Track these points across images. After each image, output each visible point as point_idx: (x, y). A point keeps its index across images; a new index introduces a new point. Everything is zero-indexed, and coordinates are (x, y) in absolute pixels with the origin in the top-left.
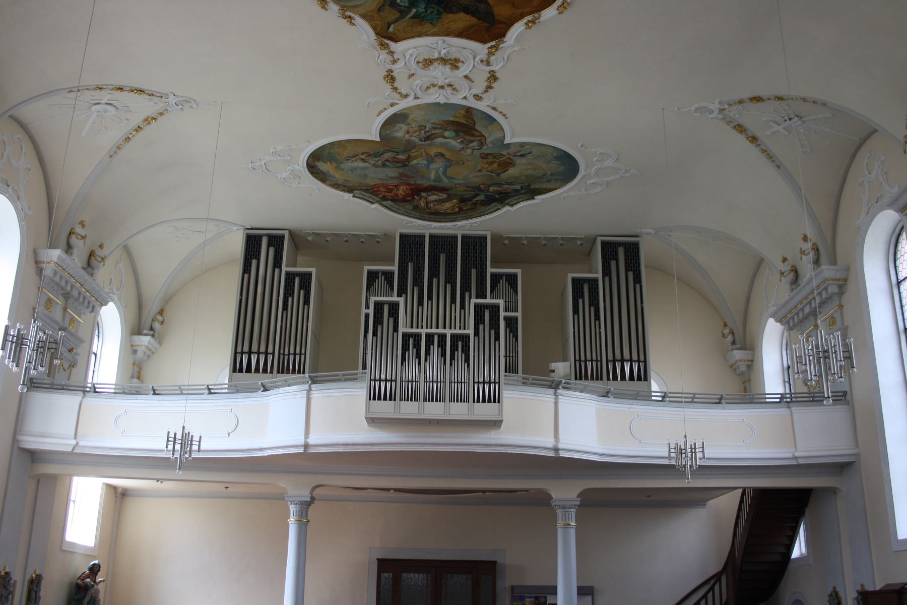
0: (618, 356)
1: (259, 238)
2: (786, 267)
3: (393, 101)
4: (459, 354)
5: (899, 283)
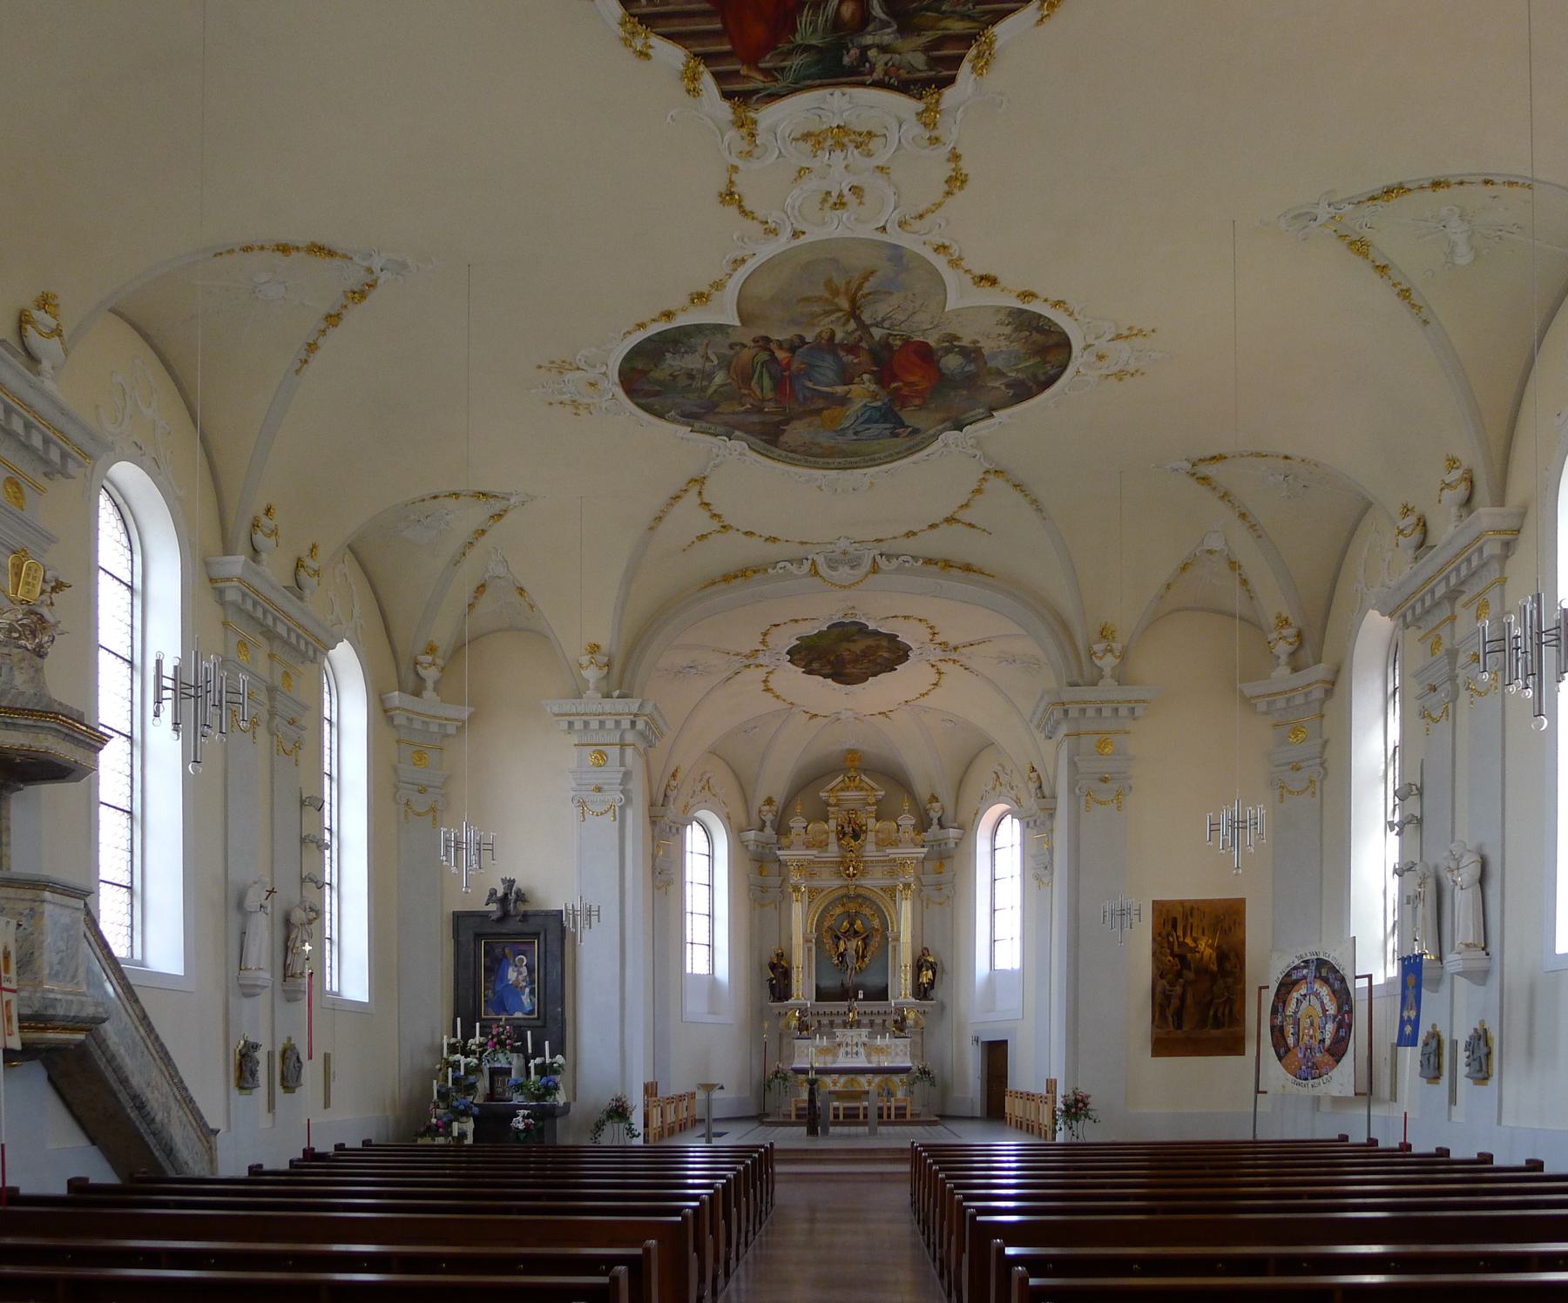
5: (995, 880)
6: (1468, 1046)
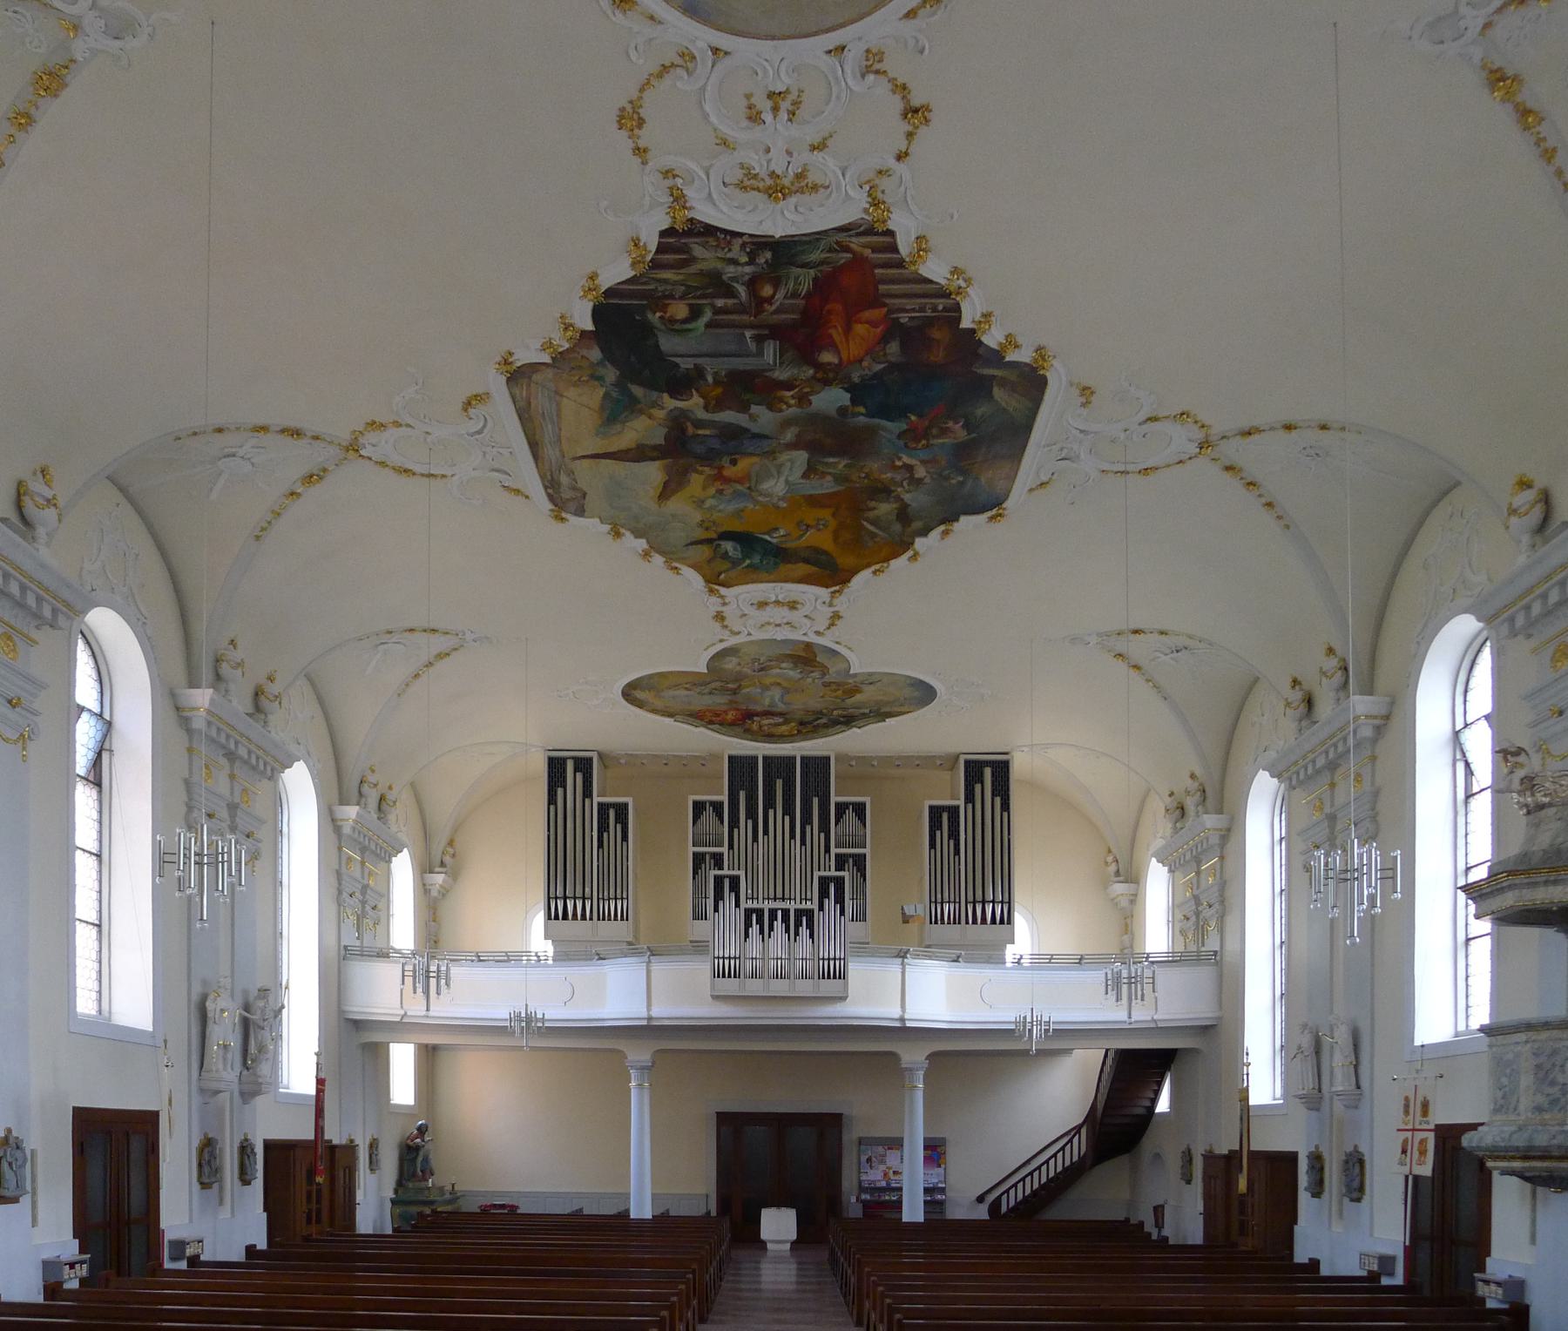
0: (979, 897)
1: (563, 761)
3: (722, 637)
4: (804, 931)
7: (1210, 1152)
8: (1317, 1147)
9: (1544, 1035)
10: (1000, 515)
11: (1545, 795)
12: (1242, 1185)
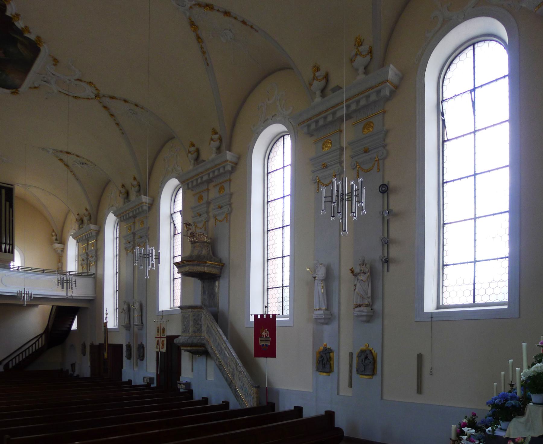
2: (192, 149)
6: (359, 356)
7: (92, 344)
8: (129, 343)
9: (196, 310)
10: (16, 93)
11: (196, 239)
12: (106, 355)
